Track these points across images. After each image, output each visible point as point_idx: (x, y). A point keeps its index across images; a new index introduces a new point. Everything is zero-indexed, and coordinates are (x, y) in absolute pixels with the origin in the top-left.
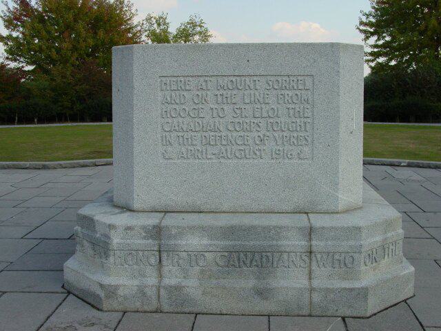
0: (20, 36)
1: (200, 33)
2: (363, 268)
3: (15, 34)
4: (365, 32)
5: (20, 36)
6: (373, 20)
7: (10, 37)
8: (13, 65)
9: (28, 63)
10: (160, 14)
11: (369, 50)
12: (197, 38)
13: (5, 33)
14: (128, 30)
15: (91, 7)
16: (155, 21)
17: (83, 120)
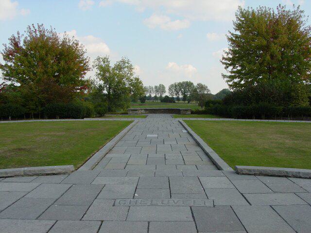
0: (13, 65)
1: (128, 67)
2: (206, 92)
3: (9, 64)
4: (226, 64)
5: (13, 65)
6: (231, 57)
7: (6, 65)
8: (9, 83)
9: (17, 81)
10: (105, 57)
11: (229, 74)
12: (126, 69)
13: (3, 63)
14: (80, 62)
15: (58, 47)
16: (102, 60)
17: (42, 118)
